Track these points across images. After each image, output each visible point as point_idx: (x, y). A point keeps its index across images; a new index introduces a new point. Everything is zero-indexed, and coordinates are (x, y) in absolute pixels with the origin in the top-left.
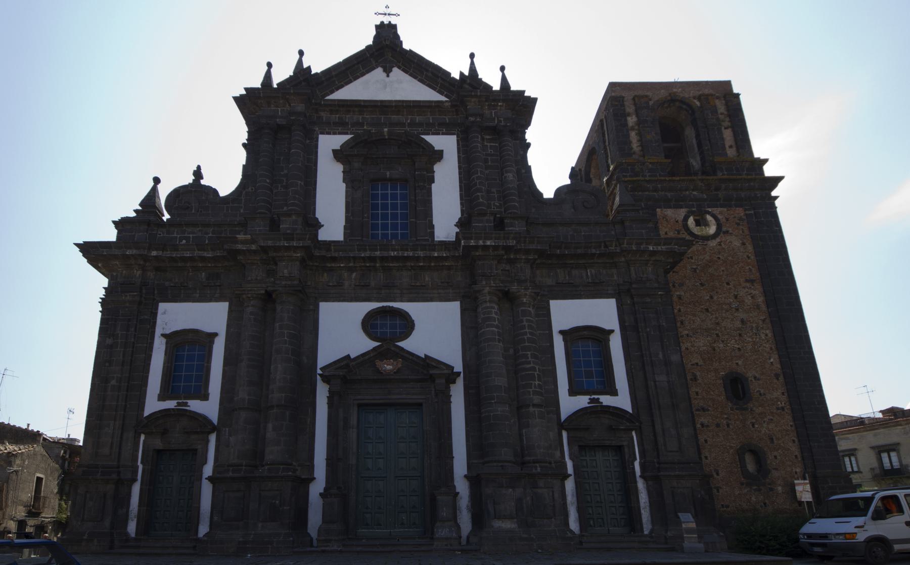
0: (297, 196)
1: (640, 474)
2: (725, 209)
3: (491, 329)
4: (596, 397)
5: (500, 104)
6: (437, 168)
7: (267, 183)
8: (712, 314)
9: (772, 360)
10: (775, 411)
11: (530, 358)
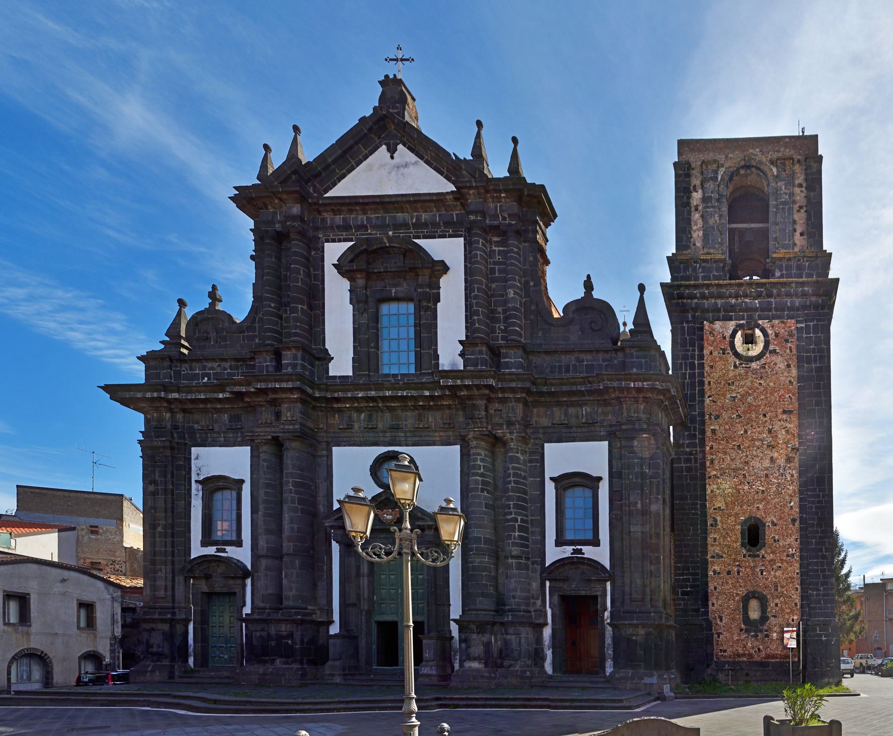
0: (298, 324)
1: (444, 282)
3: (476, 478)
4: (579, 547)
5: (502, 195)
6: (443, 281)
7: (633, 477)
8: (743, 452)
9: (792, 504)
10: (785, 558)
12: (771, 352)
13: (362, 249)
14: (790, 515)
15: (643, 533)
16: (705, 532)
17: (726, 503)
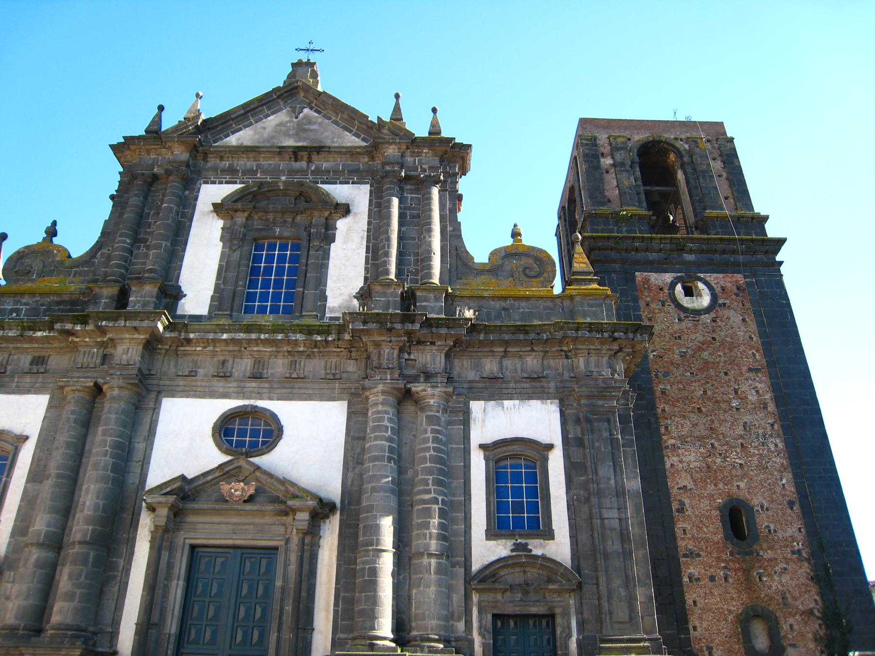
1: (342, 225)
2: (721, 276)
4: (523, 541)
9: (784, 481)
10: (789, 556)
11: (431, 485)
12: (720, 305)
13: (251, 190)
14: (784, 496)
15: (620, 520)
16: (672, 522)
17: (694, 481)
